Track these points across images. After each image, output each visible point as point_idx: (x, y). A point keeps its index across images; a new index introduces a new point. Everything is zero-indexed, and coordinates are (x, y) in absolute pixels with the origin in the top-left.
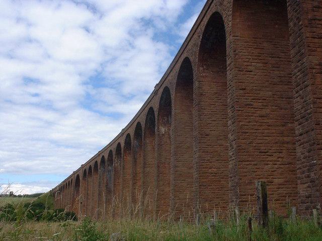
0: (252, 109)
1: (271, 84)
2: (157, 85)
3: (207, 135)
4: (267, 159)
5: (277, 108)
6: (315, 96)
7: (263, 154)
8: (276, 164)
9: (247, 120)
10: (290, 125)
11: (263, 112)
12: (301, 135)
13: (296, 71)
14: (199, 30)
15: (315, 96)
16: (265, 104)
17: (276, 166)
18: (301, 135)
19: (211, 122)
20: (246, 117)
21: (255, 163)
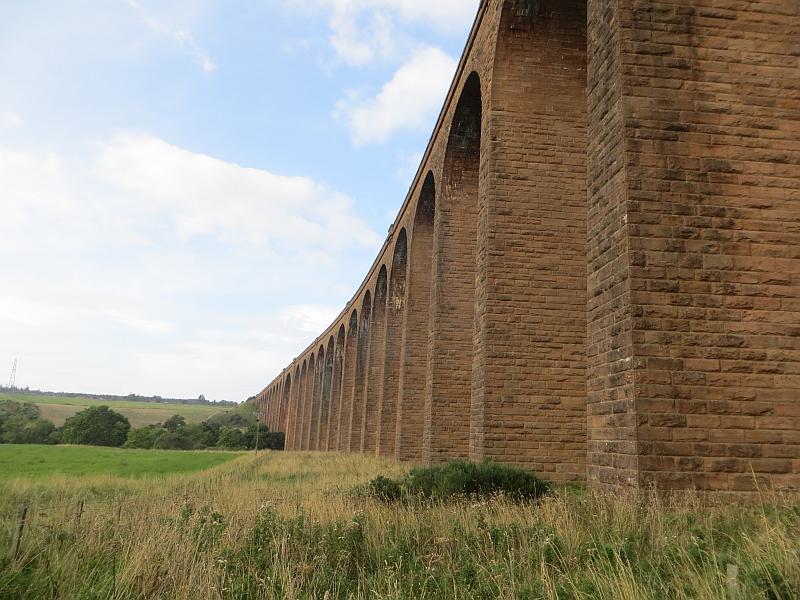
0: (523, 254)
1: (564, 204)
2: (392, 226)
3: (452, 309)
4: (548, 356)
5: (574, 252)
6: (636, 193)
7: (541, 344)
9: (510, 276)
11: (545, 260)
12: (598, 293)
13: (596, 141)
14: (448, 115)
15: (636, 193)
16: (549, 245)
18: (598, 293)
20: (508, 270)
21: (523, 361)
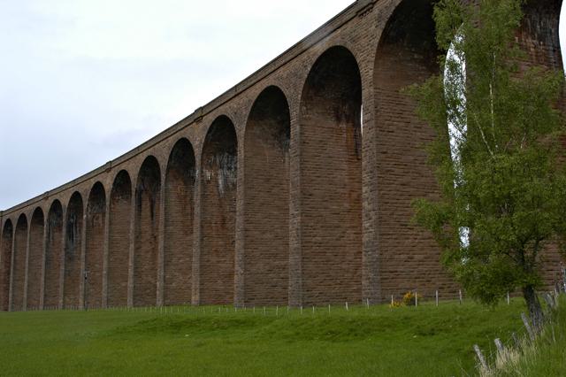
2: (201, 108)
8: (408, 239)
10: (431, 195)
11: (405, 180)
17: (417, 241)
19: (314, 178)
